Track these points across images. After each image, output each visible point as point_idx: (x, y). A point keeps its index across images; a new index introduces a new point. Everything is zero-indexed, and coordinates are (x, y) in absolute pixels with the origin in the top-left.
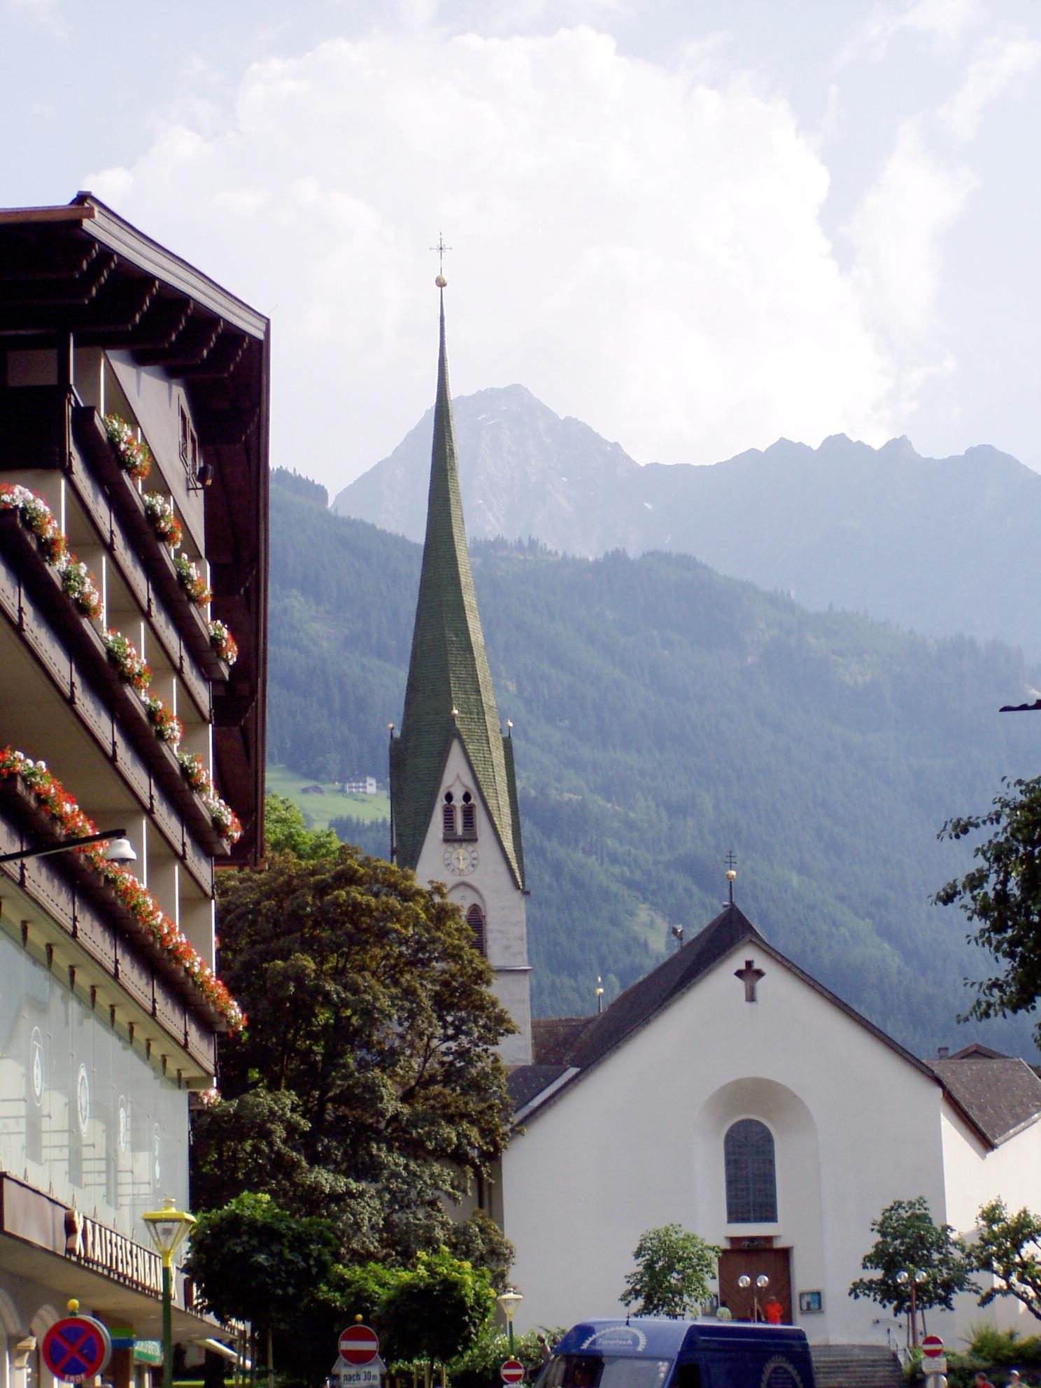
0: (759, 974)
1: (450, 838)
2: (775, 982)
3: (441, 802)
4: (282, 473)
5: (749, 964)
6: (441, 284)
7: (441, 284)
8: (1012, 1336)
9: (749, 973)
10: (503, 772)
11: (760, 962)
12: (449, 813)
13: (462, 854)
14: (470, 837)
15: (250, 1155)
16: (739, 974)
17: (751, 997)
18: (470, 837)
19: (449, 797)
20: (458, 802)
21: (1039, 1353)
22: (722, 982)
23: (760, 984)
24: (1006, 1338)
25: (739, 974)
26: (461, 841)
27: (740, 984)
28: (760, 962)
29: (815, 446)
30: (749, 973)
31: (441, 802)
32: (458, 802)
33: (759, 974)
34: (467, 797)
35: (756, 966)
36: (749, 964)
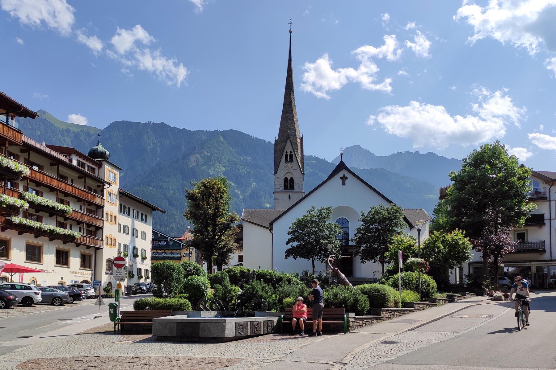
0: (347, 178)
1: (286, 161)
2: (351, 179)
3: (285, 153)
4: (311, 158)
5: (344, 176)
6: (290, 32)
7: (290, 32)
9: (344, 178)
10: (416, 326)
11: (347, 175)
12: (286, 156)
13: (289, 165)
14: (291, 161)
17: (344, 184)
18: (291, 161)
19: (287, 152)
20: (289, 154)
22: (337, 179)
26: (289, 162)
29: (95, 36)
30: (344, 178)
31: (285, 152)
32: (289, 154)
34: (291, 152)
35: (346, 176)
36: (344, 176)
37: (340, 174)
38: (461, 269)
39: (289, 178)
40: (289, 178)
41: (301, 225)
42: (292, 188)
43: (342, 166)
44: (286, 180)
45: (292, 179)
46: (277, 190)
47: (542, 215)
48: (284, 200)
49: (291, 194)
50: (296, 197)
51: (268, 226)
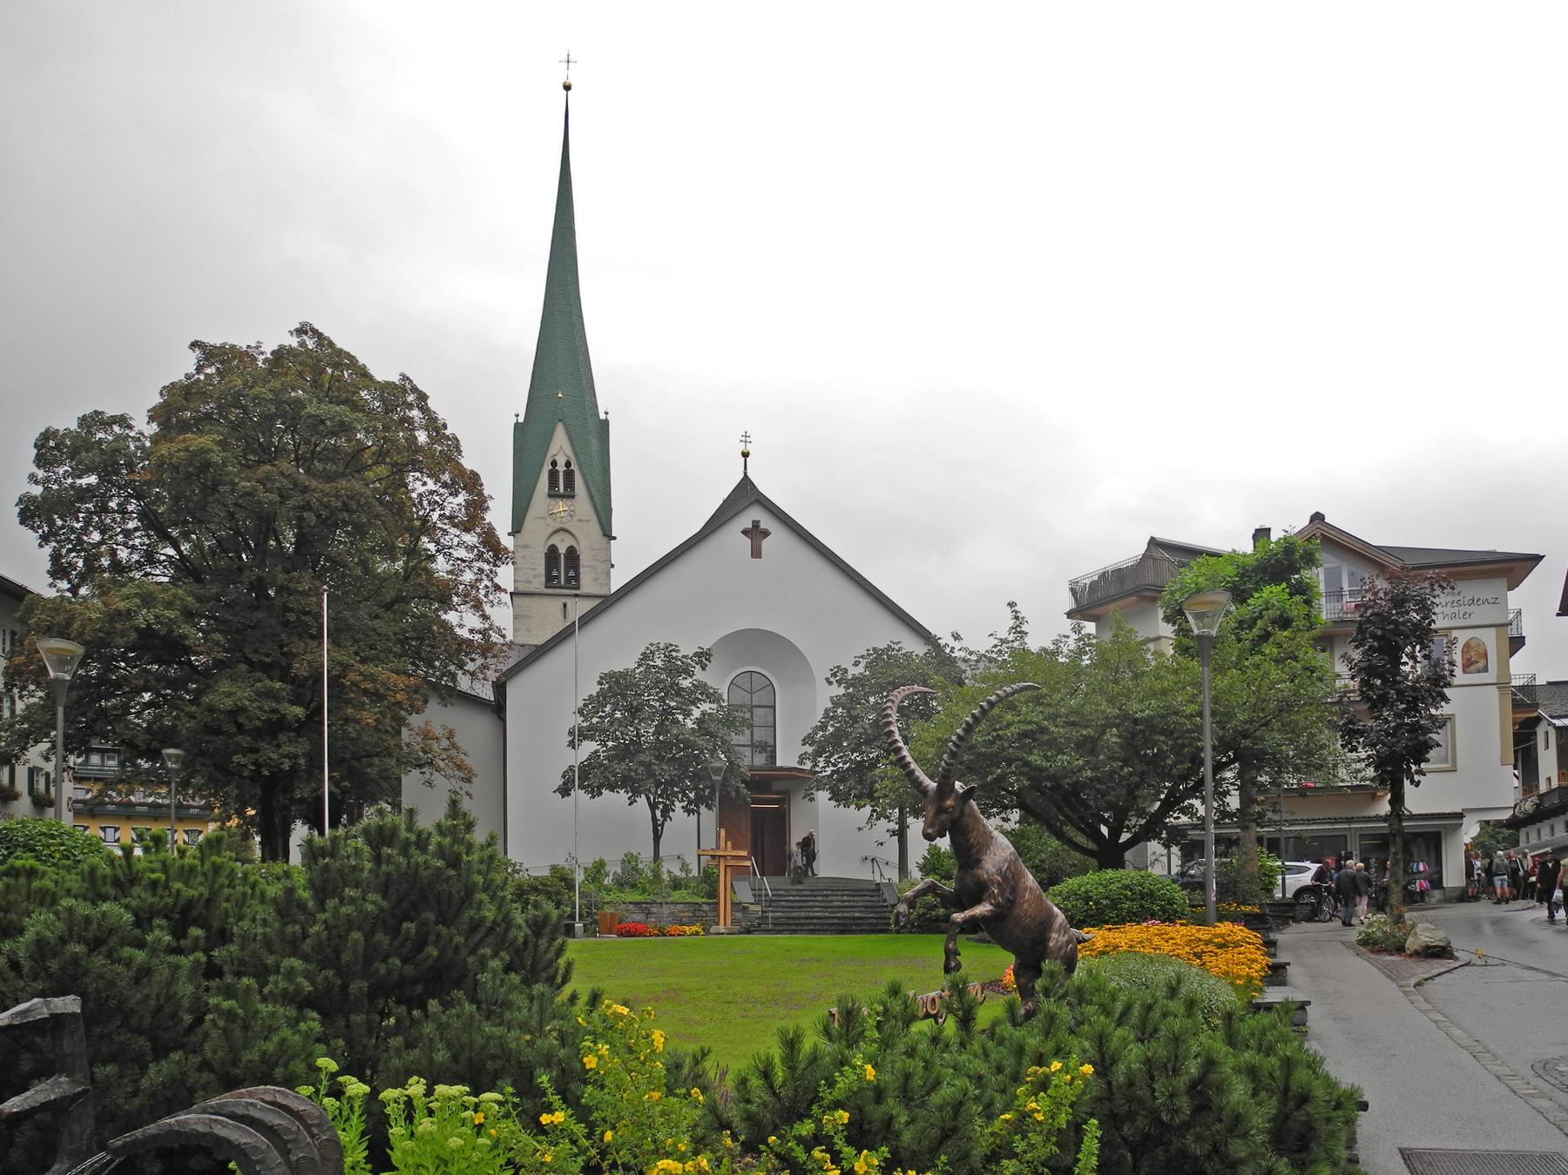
0: (766, 534)
1: (553, 494)
2: (777, 541)
3: (547, 467)
5: (756, 524)
6: (567, 88)
8: (1261, 534)
9: (756, 534)
11: (766, 522)
12: (553, 475)
13: (561, 506)
14: (570, 495)
15: (206, 640)
16: (745, 532)
17: (756, 553)
18: (570, 495)
19: (554, 463)
20: (561, 468)
21: (1268, 718)
22: (733, 537)
23: (766, 543)
24: (1247, 547)
25: (745, 532)
26: (562, 497)
27: (746, 542)
28: (766, 522)
30: (756, 534)
32: (561, 468)
33: (766, 534)
34: (568, 464)
35: (763, 526)
36: (756, 524)
37: (745, 520)
38: (13, 712)
39: (562, 550)
40: (562, 550)
41: (616, 686)
42: (574, 581)
43: (745, 494)
44: (552, 555)
45: (572, 555)
46: (521, 588)
47: (1203, 842)
48: (549, 617)
49: (570, 602)
50: (579, 608)
51: (487, 693)
